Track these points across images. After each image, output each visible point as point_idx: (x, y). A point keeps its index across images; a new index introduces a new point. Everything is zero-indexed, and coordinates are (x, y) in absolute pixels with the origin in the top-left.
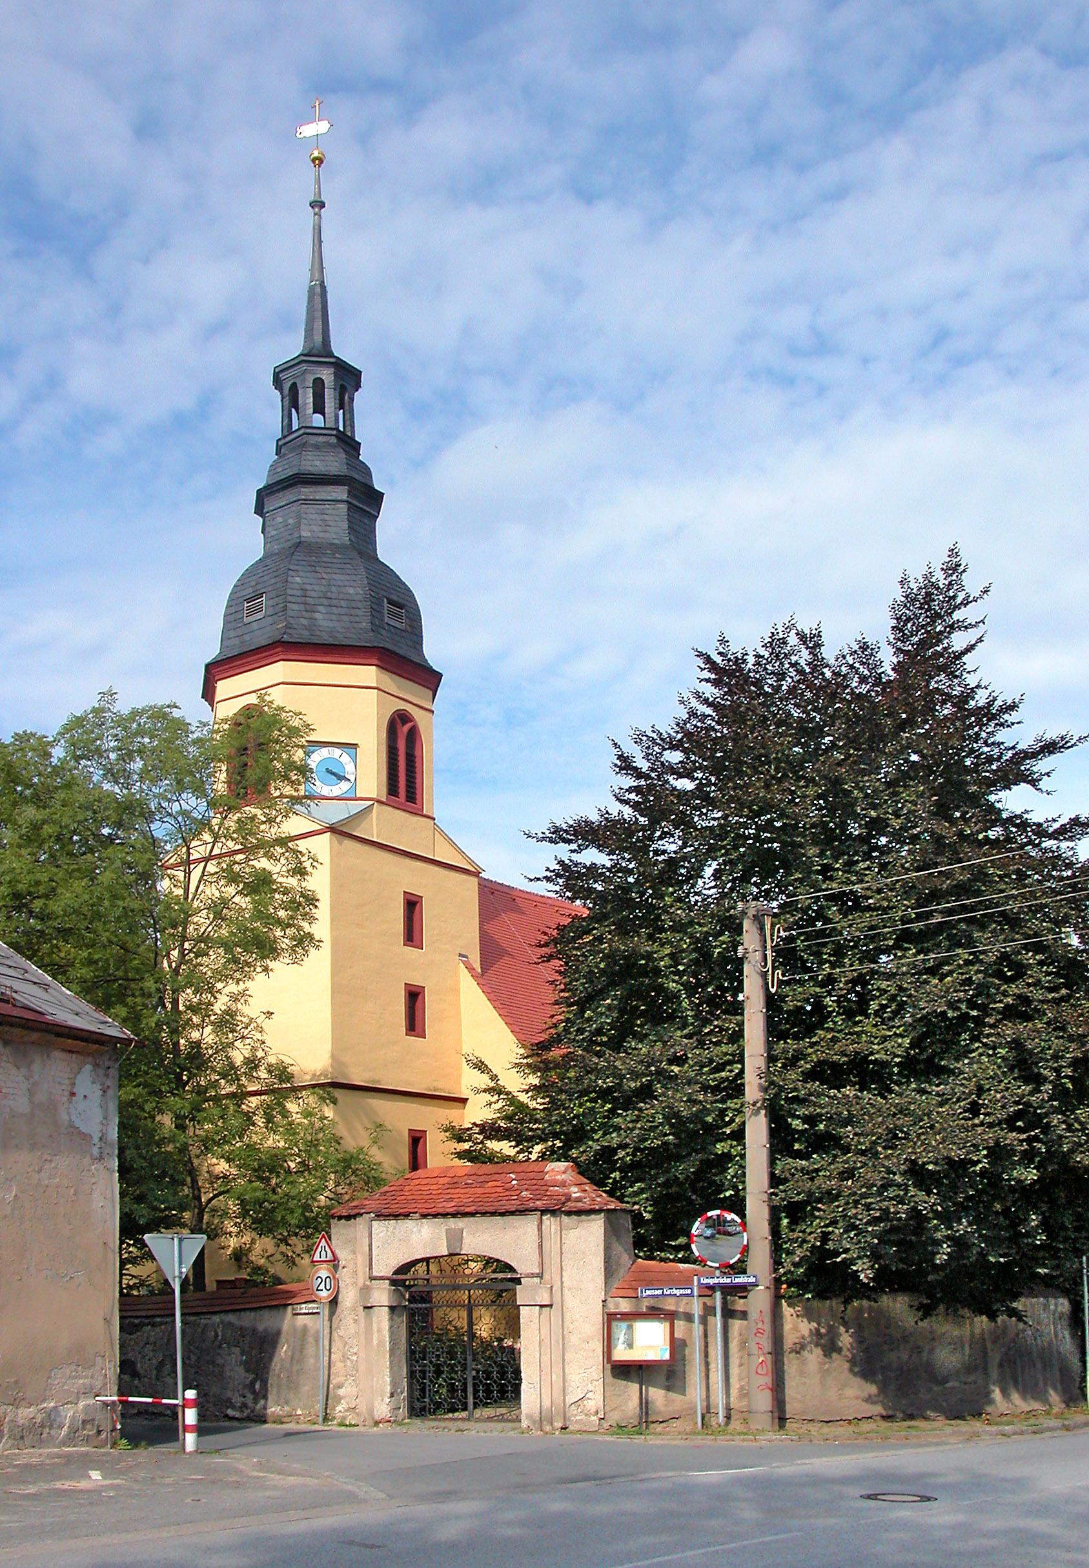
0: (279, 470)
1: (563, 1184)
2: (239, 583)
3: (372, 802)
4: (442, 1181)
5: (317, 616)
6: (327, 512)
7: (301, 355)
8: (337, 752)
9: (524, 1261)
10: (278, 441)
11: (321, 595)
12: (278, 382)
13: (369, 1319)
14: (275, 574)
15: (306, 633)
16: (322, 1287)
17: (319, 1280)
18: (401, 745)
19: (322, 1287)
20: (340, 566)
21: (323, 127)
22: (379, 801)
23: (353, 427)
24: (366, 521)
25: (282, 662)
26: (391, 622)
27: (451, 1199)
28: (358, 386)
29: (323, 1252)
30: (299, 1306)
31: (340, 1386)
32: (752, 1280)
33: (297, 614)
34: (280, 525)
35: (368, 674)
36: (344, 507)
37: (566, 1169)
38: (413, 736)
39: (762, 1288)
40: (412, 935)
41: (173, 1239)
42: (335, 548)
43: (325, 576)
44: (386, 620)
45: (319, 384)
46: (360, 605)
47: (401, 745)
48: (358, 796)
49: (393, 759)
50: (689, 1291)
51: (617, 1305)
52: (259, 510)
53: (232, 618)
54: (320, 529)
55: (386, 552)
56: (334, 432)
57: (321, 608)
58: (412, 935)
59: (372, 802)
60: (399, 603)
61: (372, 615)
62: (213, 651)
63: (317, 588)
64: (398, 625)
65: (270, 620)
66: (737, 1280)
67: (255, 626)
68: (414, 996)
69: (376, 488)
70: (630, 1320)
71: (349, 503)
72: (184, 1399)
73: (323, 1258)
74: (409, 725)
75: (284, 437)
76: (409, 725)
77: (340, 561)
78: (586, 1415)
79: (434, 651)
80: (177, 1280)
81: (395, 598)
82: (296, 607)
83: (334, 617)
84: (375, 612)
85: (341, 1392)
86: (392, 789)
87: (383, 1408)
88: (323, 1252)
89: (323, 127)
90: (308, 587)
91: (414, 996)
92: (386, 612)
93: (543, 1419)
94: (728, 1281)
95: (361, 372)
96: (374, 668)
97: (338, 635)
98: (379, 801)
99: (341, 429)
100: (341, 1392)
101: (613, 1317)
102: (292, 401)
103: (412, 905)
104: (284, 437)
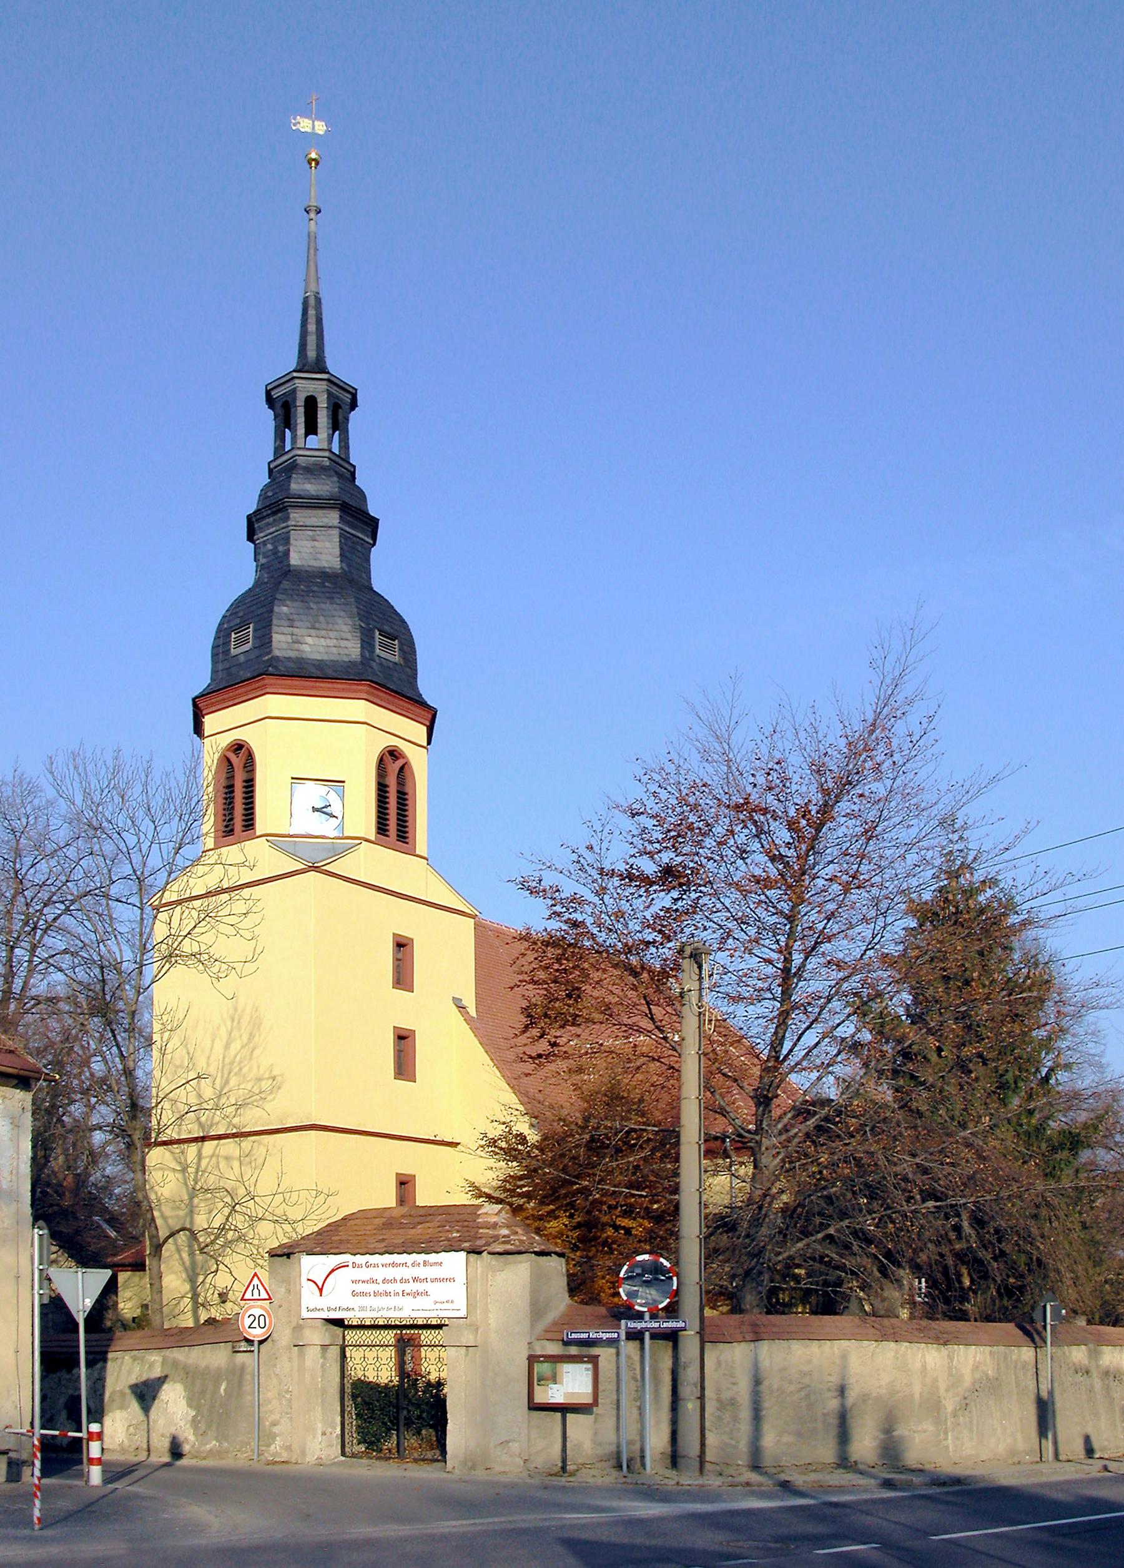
0: (270, 494)
1: (495, 1226)
2: (228, 614)
3: (359, 841)
4: (377, 1221)
6: (318, 538)
7: (294, 371)
10: (269, 463)
12: (270, 401)
13: (301, 1355)
16: (255, 1324)
17: (252, 1318)
19: (255, 1324)
21: (320, 128)
22: (367, 840)
23: (347, 447)
25: (268, 696)
27: (383, 1240)
28: (354, 405)
29: (256, 1291)
30: (238, 1344)
31: (274, 1424)
32: (681, 1324)
34: (270, 553)
35: (358, 708)
36: (336, 532)
37: (500, 1211)
38: (404, 771)
39: (693, 1333)
40: (403, 978)
42: (325, 575)
44: (378, 651)
48: (346, 834)
50: (616, 1335)
51: (543, 1348)
52: (251, 536)
55: (381, 582)
56: (327, 454)
57: (309, 640)
58: (403, 978)
59: (359, 841)
62: (202, 679)
66: (665, 1325)
68: (403, 1038)
69: (372, 514)
70: (556, 1362)
71: (339, 528)
72: (88, 1432)
73: (256, 1296)
74: (400, 763)
75: (275, 460)
76: (400, 763)
77: (330, 590)
78: (511, 1456)
79: (427, 687)
80: (81, 1313)
81: (386, 628)
85: (275, 1429)
86: (382, 828)
87: (1082, 1457)
88: (256, 1291)
89: (320, 128)
90: (295, 617)
91: (403, 1038)
92: (377, 643)
93: (471, 1463)
94: (657, 1325)
98: (367, 840)
99: (336, 450)
100: (275, 1429)
101: (536, 1359)
102: (285, 420)
103: (402, 945)
104: (275, 460)
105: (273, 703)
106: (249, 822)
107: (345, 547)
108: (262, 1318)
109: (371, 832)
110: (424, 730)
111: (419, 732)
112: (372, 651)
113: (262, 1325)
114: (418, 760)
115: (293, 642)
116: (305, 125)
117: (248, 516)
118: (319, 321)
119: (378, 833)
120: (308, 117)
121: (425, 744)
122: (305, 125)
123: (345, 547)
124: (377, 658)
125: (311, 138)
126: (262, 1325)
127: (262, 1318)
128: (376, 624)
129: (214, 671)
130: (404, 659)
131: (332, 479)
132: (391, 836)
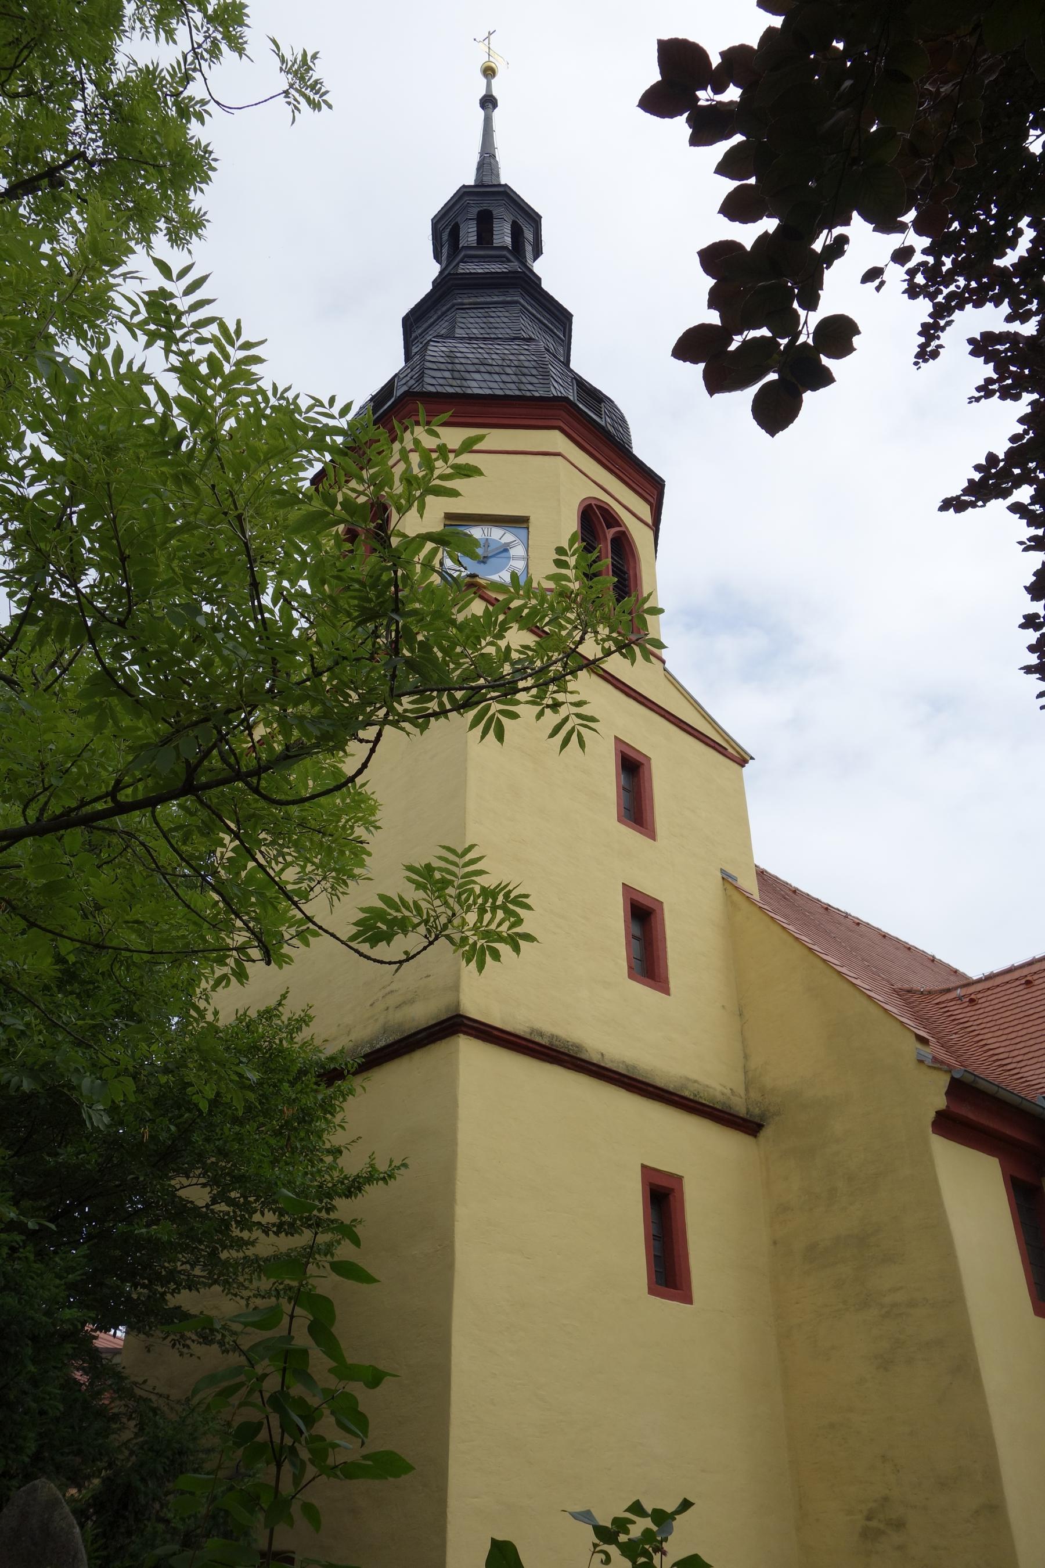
38: (623, 546)
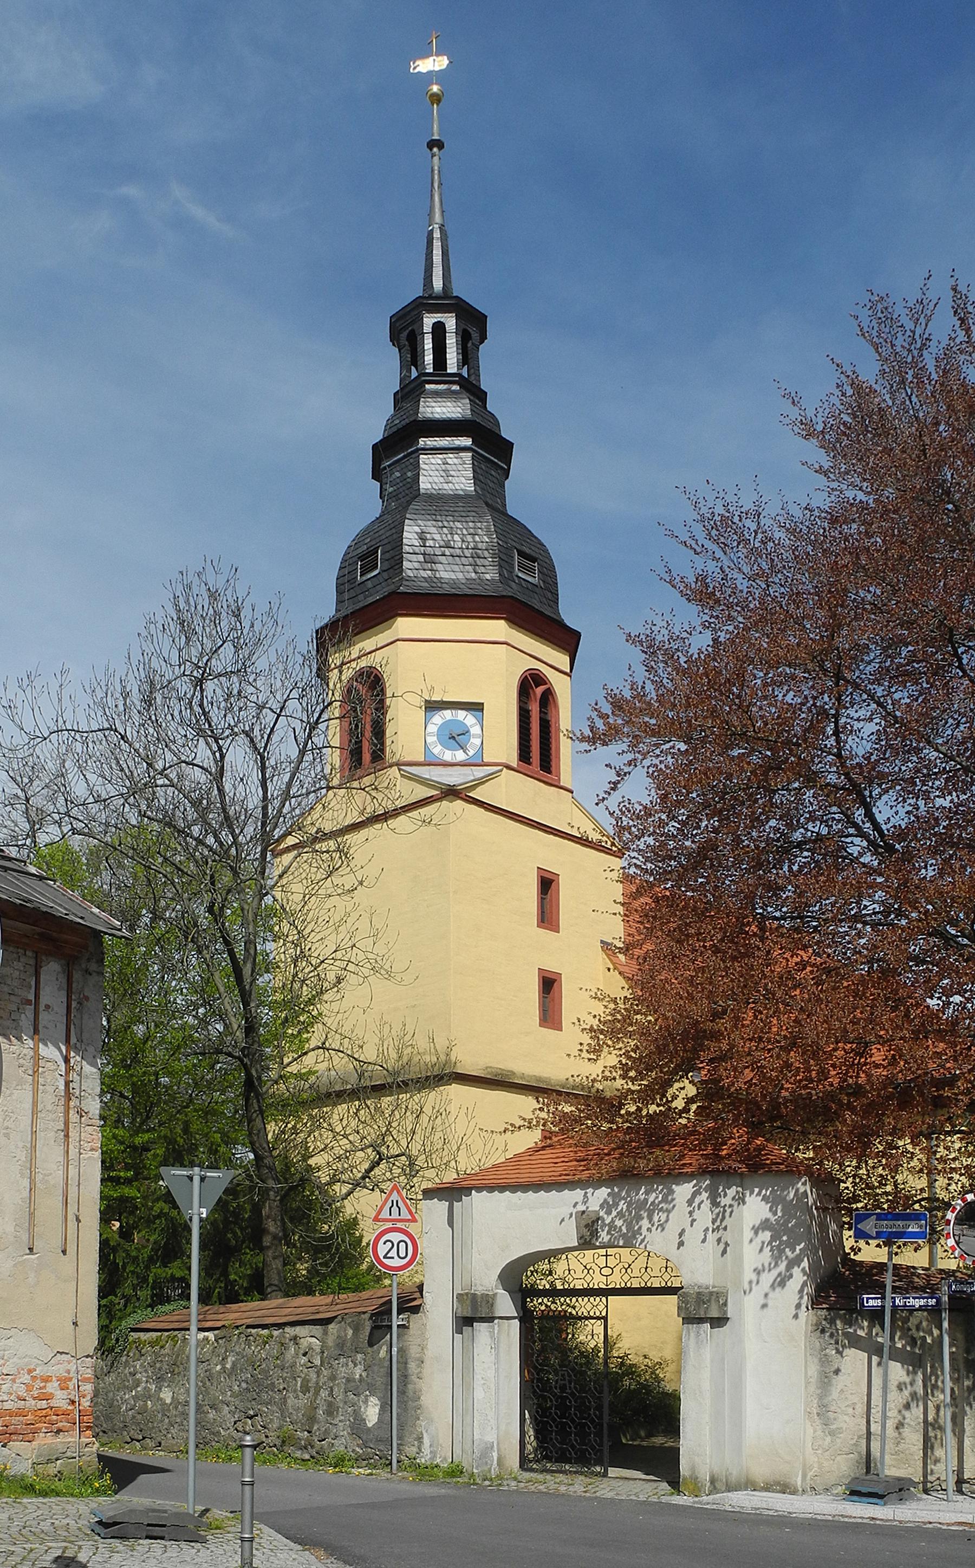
5: (439, 567)
6: (449, 461)
8: (461, 714)
9: (896, 1383)
11: (442, 543)
14: (392, 525)
15: (426, 584)
16: (393, 1253)
17: (389, 1244)
18: (534, 708)
19: (393, 1253)
20: (463, 514)
22: (509, 767)
24: (493, 473)
26: (520, 575)
28: (483, 338)
29: (395, 1209)
33: (416, 565)
35: (498, 628)
38: (548, 698)
41: (191, 1178)
43: (446, 524)
45: (439, 330)
46: (486, 554)
47: (534, 708)
49: (524, 745)
52: (377, 474)
53: (345, 583)
54: (442, 480)
57: (442, 559)
59: (500, 768)
60: (532, 557)
61: (500, 566)
62: (327, 610)
63: (437, 537)
64: (530, 579)
65: (385, 575)
67: (369, 584)
77: (461, 509)
82: (414, 557)
83: (456, 568)
84: (504, 563)
86: (524, 754)
88: (395, 1209)
95: (540, 1026)
96: (502, 622)
97: (462, 586)
98: (509, 767)
103: (547, 884)
105: (406, 625)
106: (378, 756)
107: (478, 470)
108: (402, 1245)
109: (511, 755)
110: (567, 659)
111: (562, 660)
112: (511, 572)
113: (402, 1254)
114: (561, 686)
115: (426, 562)
116: (425, 65)
117: (373, 446)
118: (487, 781)
119: (520, 760)
120: (601, 1465)
121: (568, 671)
122: (425, 65)
123: (478, 470)
124: (516, 578)
125: (430, 76)
126: (402, 1254)
127: (402, 1245)
128: (514, 544)
129: (339, 602)
130: (544, 582)
131: (463, 401)
132: (534, 764)
